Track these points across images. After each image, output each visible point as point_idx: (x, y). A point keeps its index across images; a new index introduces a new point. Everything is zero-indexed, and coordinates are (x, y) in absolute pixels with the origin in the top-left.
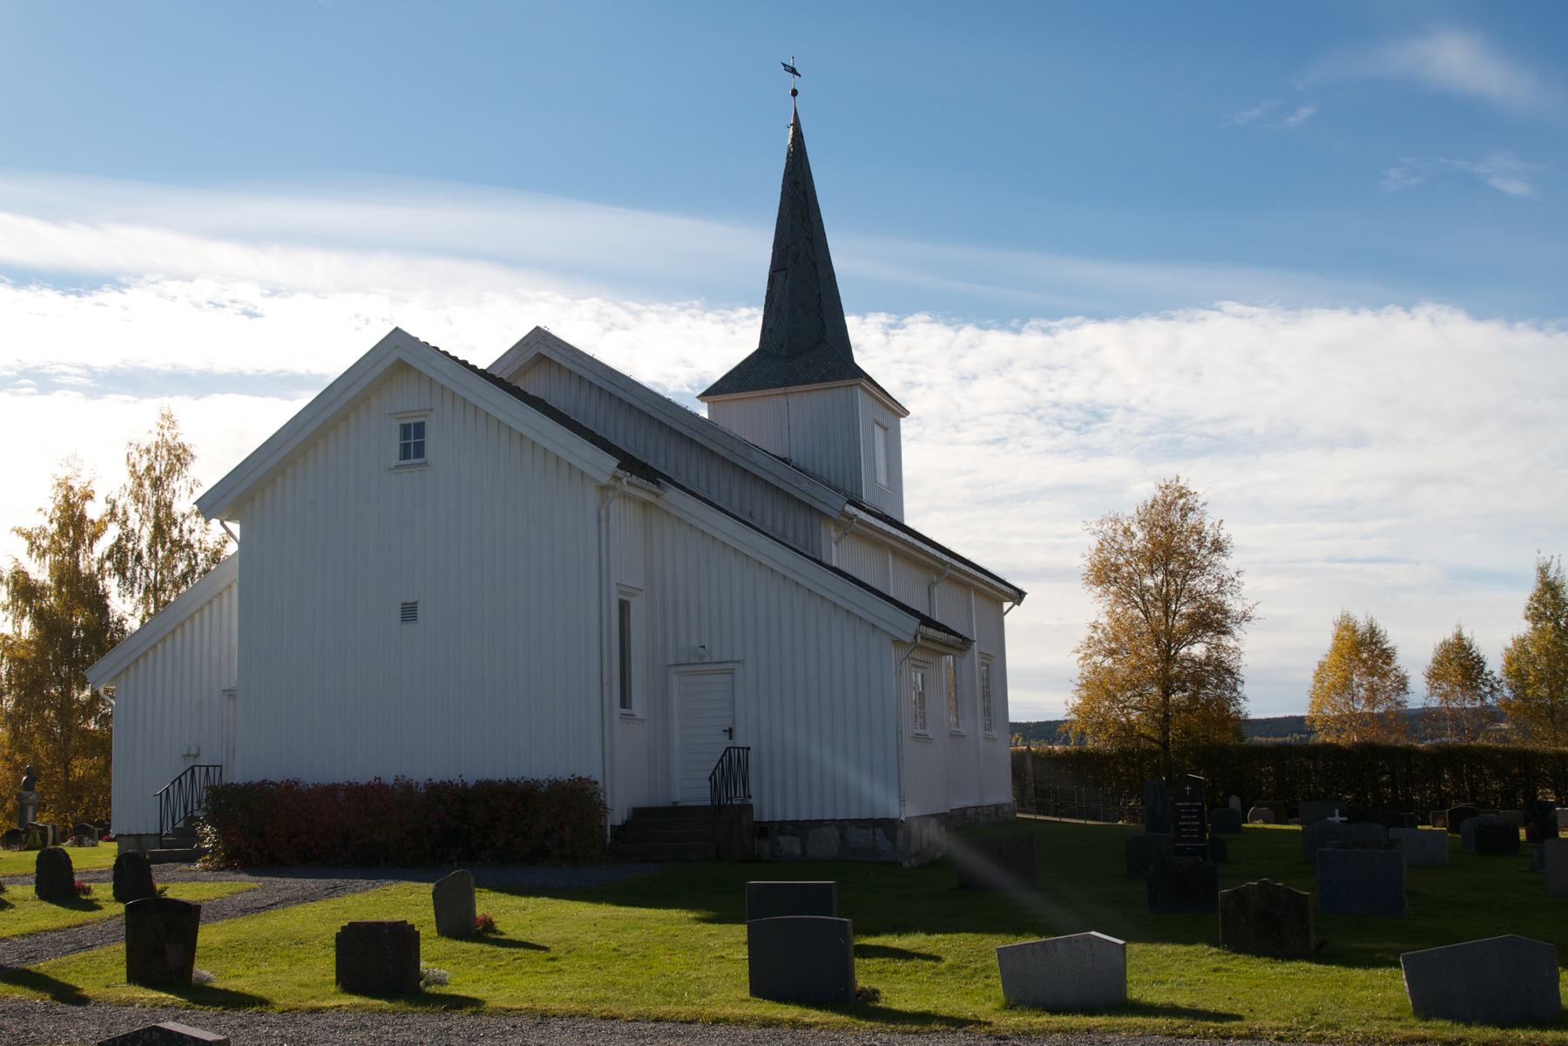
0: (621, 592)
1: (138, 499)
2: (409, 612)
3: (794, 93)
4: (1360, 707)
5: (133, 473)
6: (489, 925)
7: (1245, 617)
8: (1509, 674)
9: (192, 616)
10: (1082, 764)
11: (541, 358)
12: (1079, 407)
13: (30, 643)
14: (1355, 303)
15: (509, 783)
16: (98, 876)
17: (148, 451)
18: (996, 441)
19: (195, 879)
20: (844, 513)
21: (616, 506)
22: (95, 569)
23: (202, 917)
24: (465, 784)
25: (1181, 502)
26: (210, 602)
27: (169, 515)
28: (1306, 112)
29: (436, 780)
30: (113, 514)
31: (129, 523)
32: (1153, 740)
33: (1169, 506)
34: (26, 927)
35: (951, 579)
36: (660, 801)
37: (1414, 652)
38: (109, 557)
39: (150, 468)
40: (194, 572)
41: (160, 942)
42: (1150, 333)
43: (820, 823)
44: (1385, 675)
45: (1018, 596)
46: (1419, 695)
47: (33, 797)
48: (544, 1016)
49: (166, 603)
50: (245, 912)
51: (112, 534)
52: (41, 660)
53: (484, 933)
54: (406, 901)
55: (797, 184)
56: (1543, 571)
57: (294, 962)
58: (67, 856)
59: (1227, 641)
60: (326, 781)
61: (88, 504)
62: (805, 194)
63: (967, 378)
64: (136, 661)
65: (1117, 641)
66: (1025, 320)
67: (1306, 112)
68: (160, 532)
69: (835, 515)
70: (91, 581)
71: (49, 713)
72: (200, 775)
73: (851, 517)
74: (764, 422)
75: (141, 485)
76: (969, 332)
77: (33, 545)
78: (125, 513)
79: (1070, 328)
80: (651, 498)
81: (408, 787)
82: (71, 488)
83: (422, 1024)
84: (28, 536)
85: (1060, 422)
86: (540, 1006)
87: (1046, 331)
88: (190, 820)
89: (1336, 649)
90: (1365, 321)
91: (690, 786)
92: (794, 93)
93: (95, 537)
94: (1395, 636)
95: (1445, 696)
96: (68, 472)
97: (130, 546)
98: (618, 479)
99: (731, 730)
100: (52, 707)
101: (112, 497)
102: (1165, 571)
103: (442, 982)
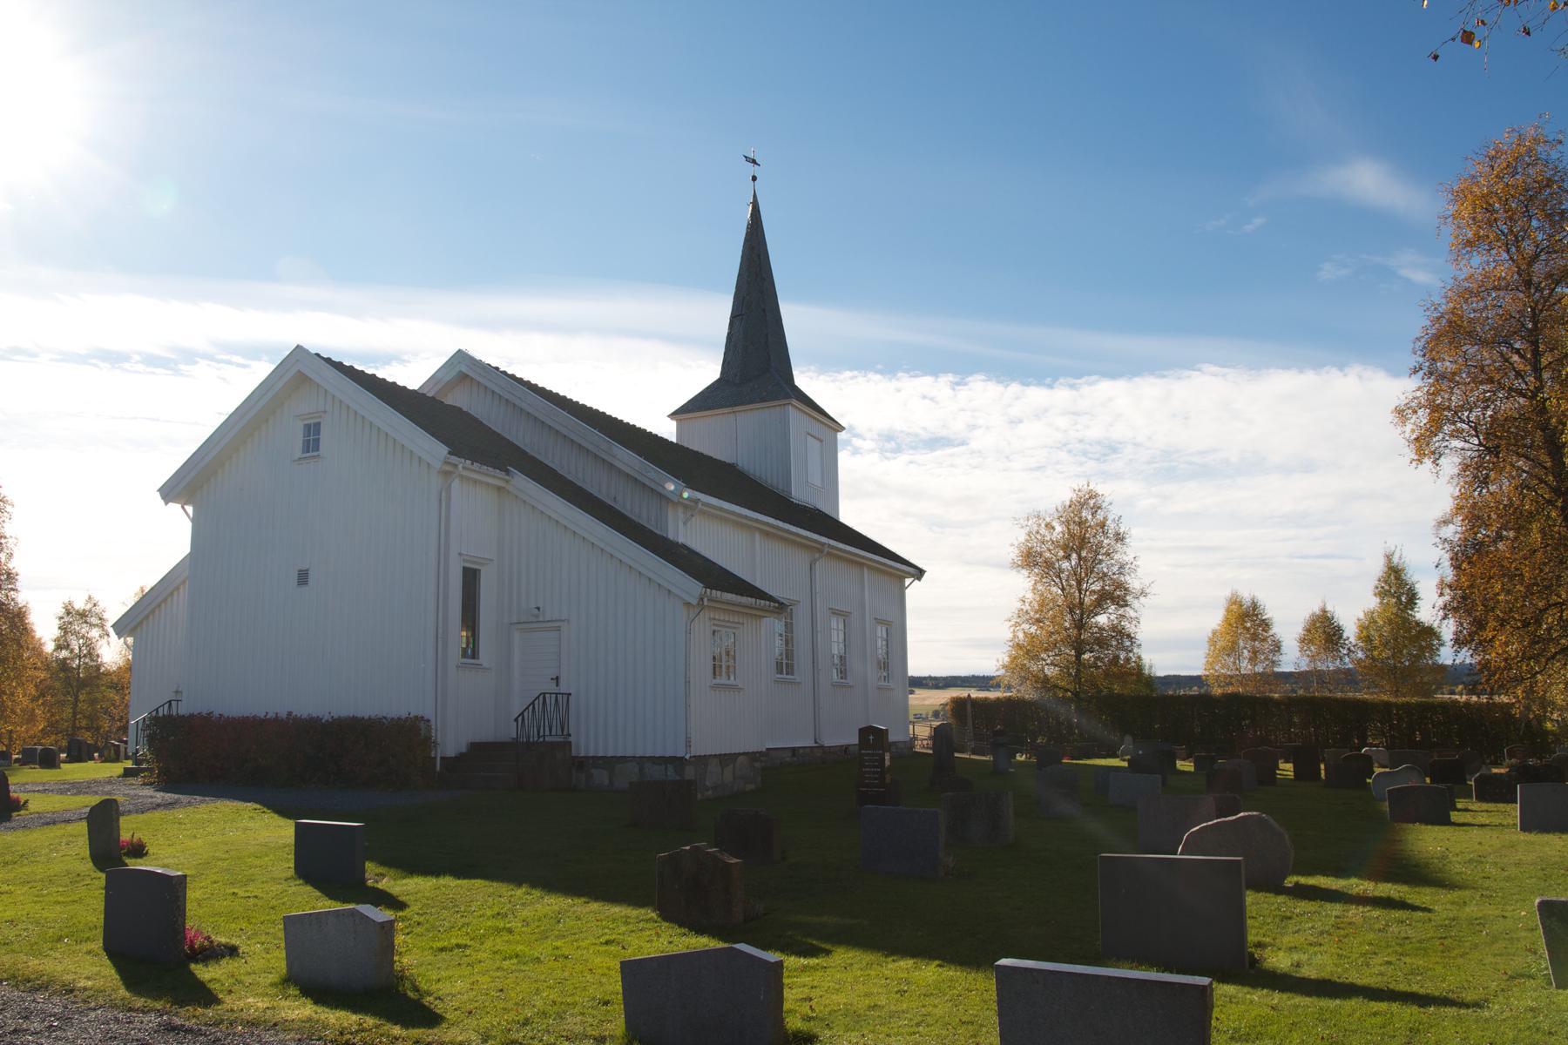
2: (303, 578)
3: (754, 178)
4: (1246, 667)
7: (1143, 593)
8: (1360, 638)
12: (1099, 443)
14: (1302, 364)
18: (1039, 468)
25: (1092, 502)
28: (1259, 221)
33: (1083, 504)
35: (829, 554)
37: (1288, 626)
42: (1149, 388)
43: (623, 759)
44: (1264, 640)
45: (919, 573)
46: (1292, 658)
56: (1389, 557)
59: (1130, 613)
63: (1015, 422)
66: (1055, 379)
67: (1259, 221)
74: (718, 439)
76: (1015, 388)
79: (1090, 384)
85: (1085, 453)
87: (1072, 387)
89: (1226, 620)
90: (1309, 378)
92: (754, 178)
94: (1271, 611)
95: (1313, 658)
102: (1079, 561)
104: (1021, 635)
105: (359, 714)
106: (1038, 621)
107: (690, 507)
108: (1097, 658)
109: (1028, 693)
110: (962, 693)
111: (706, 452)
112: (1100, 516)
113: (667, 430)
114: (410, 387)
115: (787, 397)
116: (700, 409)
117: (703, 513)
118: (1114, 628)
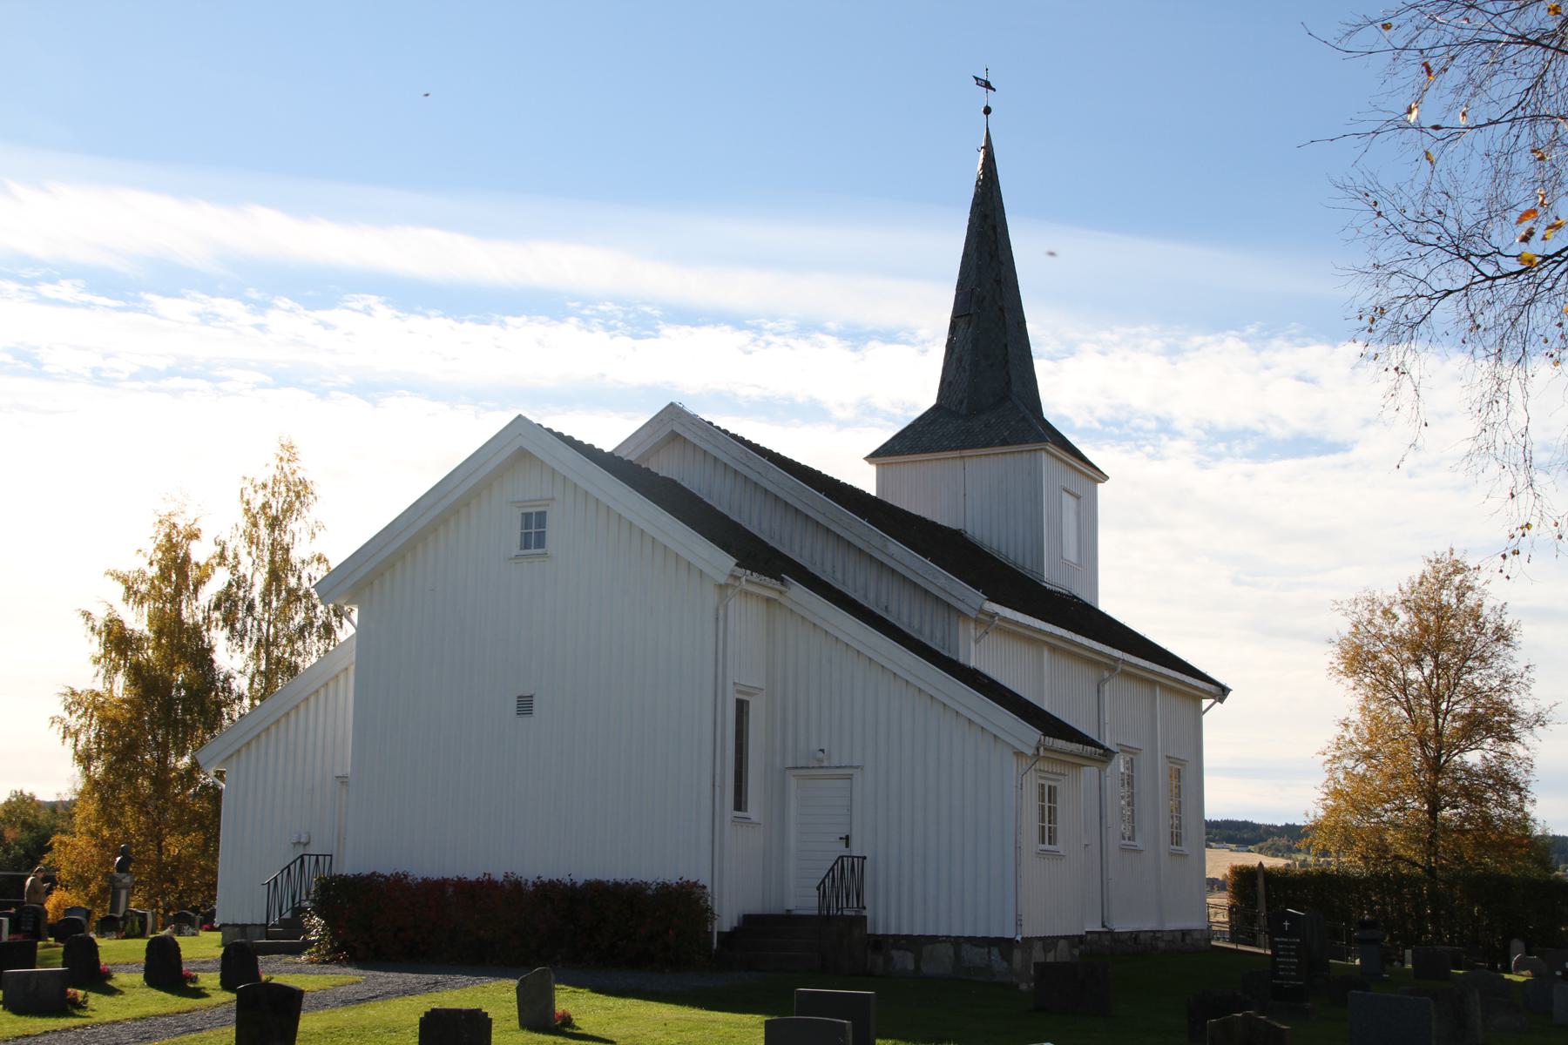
0: (739, 692)
1: (252, 540)
2: (525, 705)
3: (987, 111)
5: (247, 511)
6: (567, 1021)
7: (1539, 720)
11: (674, 436)
13: (124, 701)
16: (204, 965)
17: (265, 486)
19: (300, 971)
20: (981, 611)
22: (200, 618)
23: (305, 1005)
27: (286, 561)
29: (545, 879)
31: (240, 568)
32: (1415, 864)
36: (773, 908)
38: (217, 607)
40: (311, 624)
43: (934, 939)
45: (1222, 692)
47: (127, 880)
49: (279, 660)
50: (346, 1003)
55: (986, 216)
59: (1517, 749)
60: (436, 874)
61: (194, 544)
62: (994, 228)
64: (248, 743)
65: (1374, 742)
68: (275, 576)
69: (973, 614)
70: (195, 632)
71: (144, 783)
73: (993, 615)
75: (255, 525)
77: (130, 592)
78: (236, 556)
82: (175, 526)
84: (125, 581)
88: (298, 911)
91: (801, 898)
92: (987, 111)
93: (199, 583)
96: (172, 507)
97: (241, 594)
99: (847, 838)
102: (1434, 658)
106: (1369, 756)
107: (987, 622)
108: (1467, 818)
109: (1349, 862)
112: (1471, 600)
113: (865, 480)
117: (999, 629)
118: (1490, 772)
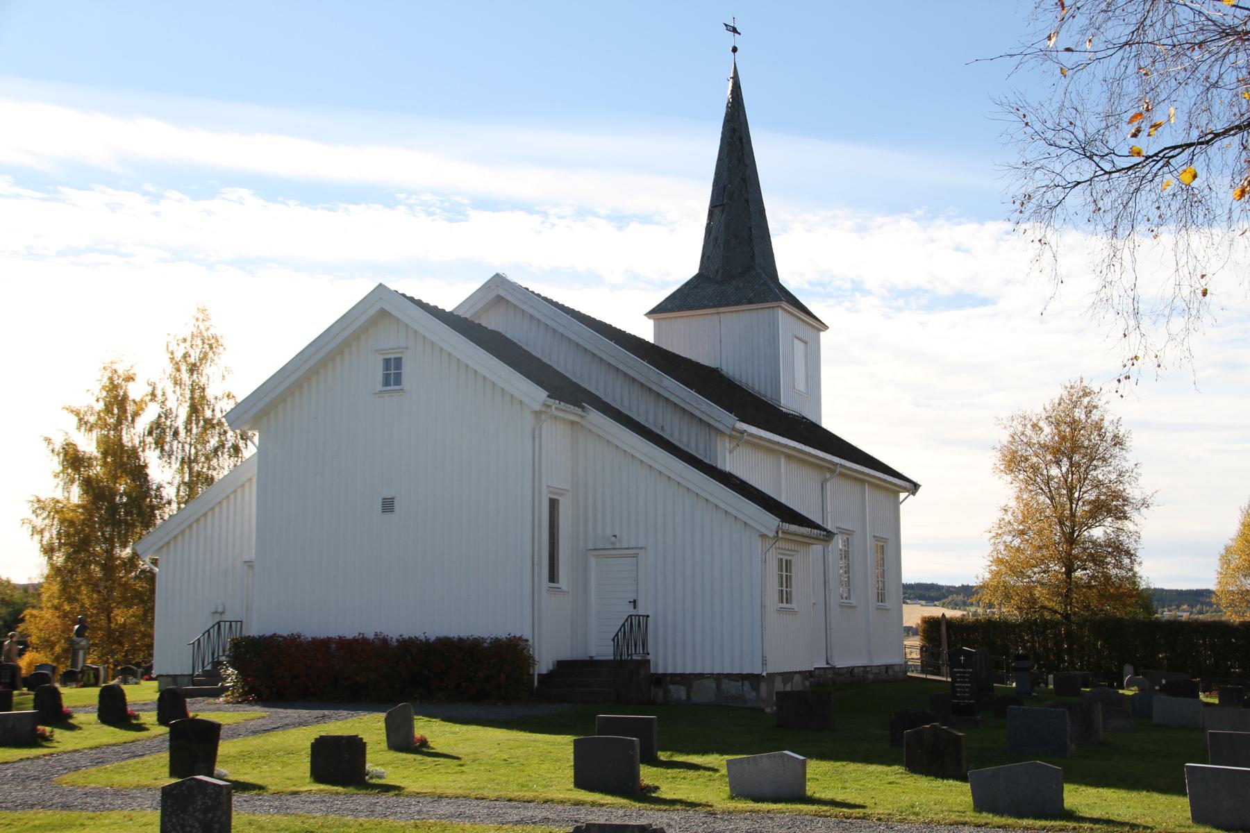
1: (177, 382)
2: (388, 505)
3: (735, 50)
6: (424, 743)
7: (1145, 503)
9: (220, 503)
10: (986, 634)
11: (500, 299)
13: (78, 506)
15: (460, 640)
16: (144, 706)
17: (185, 340)
19: (219, 710)
20: (734, 429)
21: (547, 427)
22: (137, 442)
24: (428, 640)
26: (235, 491)
27: (203, 397)
29: (406, 636)
30: (153, 395)
32: (1056, 612)
34: (92, 743)
36: (580, 655)
39: (186, 356)
40: (223, 446)
41: (194, 745)
48: (440, 797)
50: (254, 733)
51: (150, 414)
52: (89, 522)
53: (420, 748)
54: (369, 727)
55: (734, 130)
57: (285, 765)
58: (122, 691)
59: (1128, 525)
61: (131, 385)
62: (741, 139)
68: (194, 410)
69: (727, 431)
70: (134, 453)
72: (225, 628)
73: (743, 432)
74: (699, 339)
75: (178, 370)
78: (164, 394)
80: (576, 419)
81: (385, 642)
83: (362, 799)
84: (78, 414)
86: (439, 791)
88: (217, 664)
91: (600, 647)
92: (735, 50)
93: (136, 414)
97: (168, 423)
98: (549, 406)
99: (635, 601)
100: (97, 563)
101: (153, 380)
102: (1071, 462)
103: (380, 777)
104: (1002, 547)
105: (451, 635)
106: (1022, 533)
110: (936, 611)
111: (694, 358)
112: (1095, 416)
113: (645, 331)
114: (448, 310)
115: (777, 299)
116: (680, 308)
117: (747, 442)
